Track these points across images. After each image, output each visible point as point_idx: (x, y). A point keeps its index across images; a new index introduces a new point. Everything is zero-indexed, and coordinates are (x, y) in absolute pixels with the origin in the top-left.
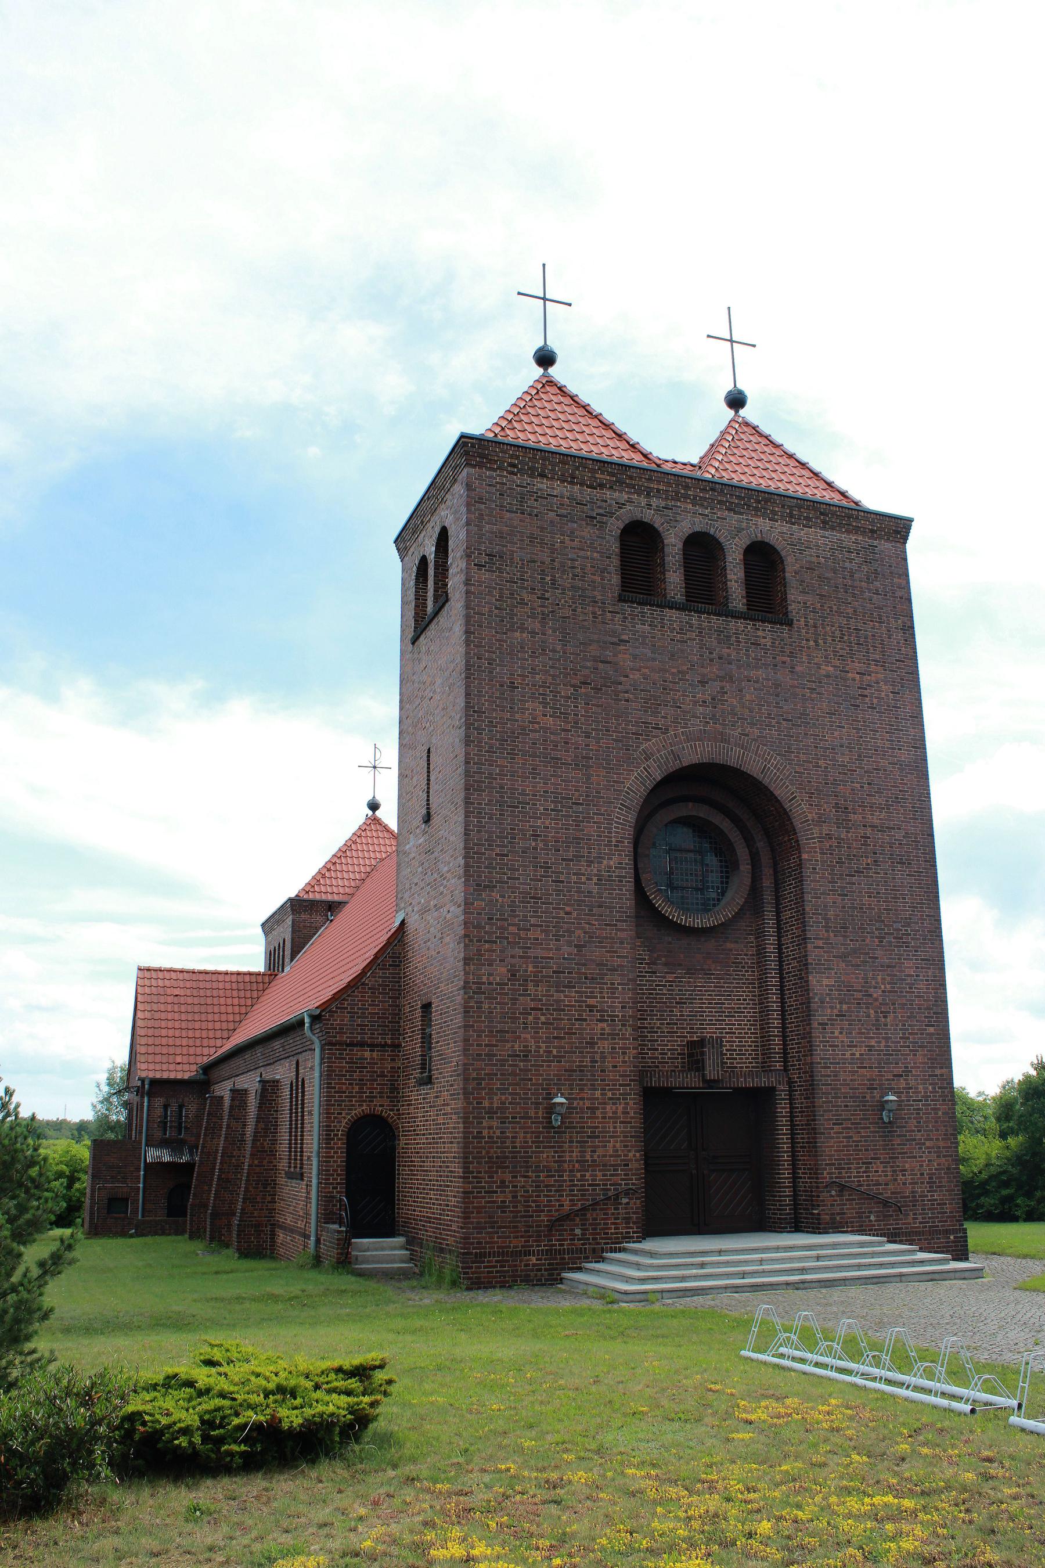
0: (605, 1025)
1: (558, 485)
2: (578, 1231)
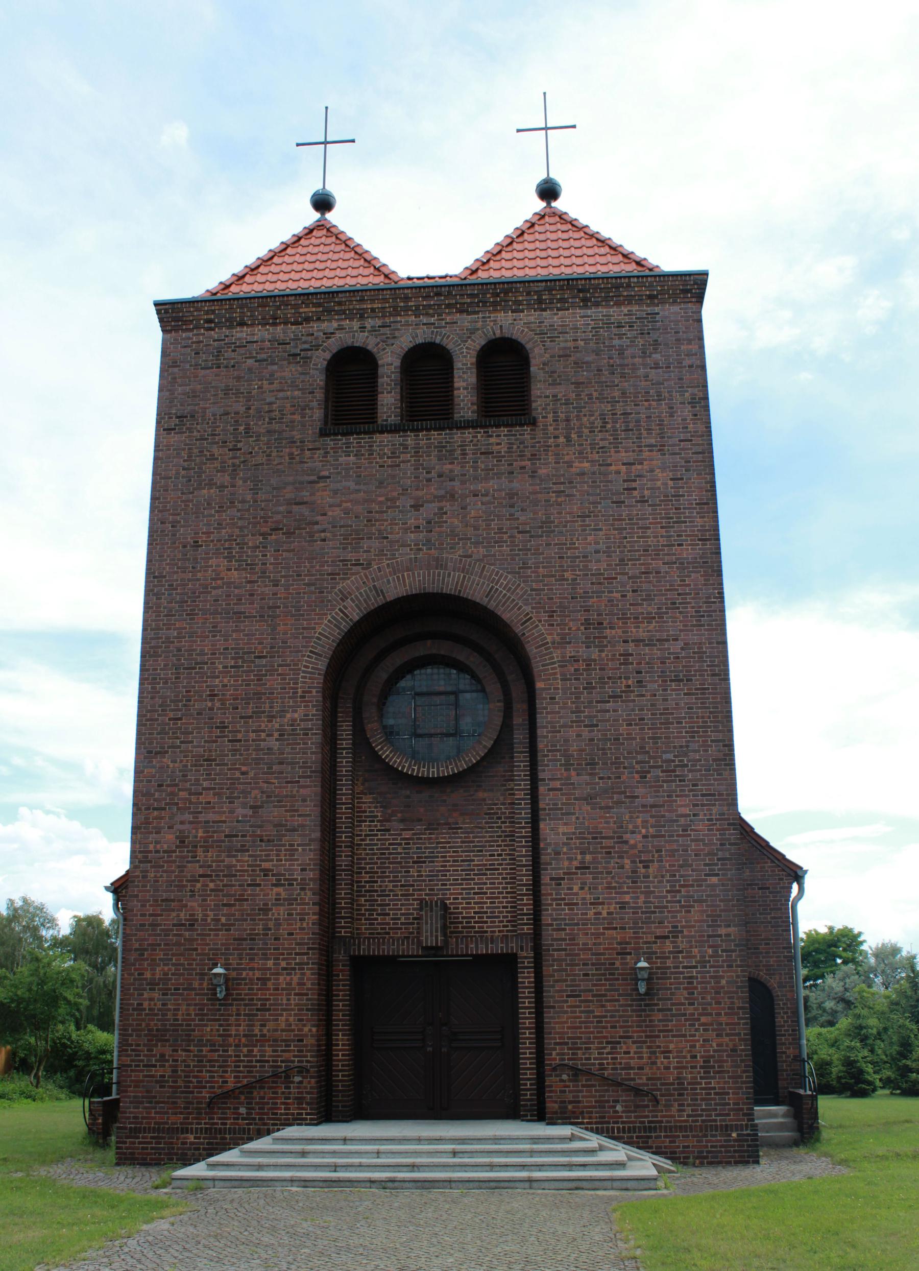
0: (281, 889)
1: (259, 330)
2: (243, 1110)
